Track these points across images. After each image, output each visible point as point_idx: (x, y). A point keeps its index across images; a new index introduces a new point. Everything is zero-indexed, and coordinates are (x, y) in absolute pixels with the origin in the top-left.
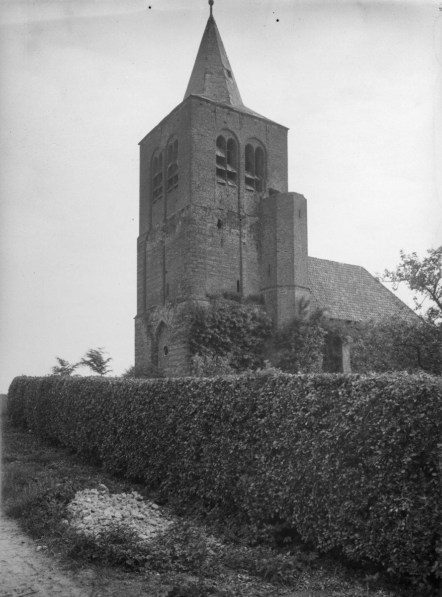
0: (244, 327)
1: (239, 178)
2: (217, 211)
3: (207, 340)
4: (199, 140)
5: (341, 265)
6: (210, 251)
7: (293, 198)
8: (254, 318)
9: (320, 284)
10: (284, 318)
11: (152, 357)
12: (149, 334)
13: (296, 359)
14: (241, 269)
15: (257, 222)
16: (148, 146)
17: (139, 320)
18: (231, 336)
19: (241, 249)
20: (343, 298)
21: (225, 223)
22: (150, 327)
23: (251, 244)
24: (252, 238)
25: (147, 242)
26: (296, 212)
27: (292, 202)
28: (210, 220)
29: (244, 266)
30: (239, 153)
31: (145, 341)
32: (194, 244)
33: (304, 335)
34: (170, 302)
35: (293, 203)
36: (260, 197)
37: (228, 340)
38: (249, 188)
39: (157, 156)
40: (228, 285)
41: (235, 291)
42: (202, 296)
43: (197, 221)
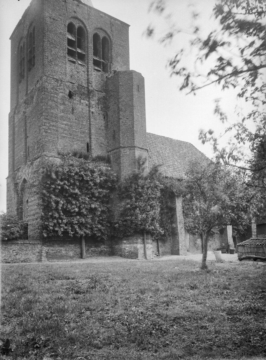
0: (91, 180)
1: (88, 59)
2: (68, 84)
3: (57, 191)
4: (51, 22)
5: (174, 140)
6: (62, 117)
7: (132, 75)
8: (101, 174)
9: (158, 152)
10: (126, 172)
11: (18, 209)
12: (16, 191)
13: (136, 207)
14: (90, 134)
15: (104, 97)
16: (16, 38)
17: (10, 180)
18: (80, 188)
19: (90, 117)
20: (176, 163)
21: (75, 94)
22: (16, 184)
23: (99, 114)
24: (100, 109)
25: (15, 115)
26: (135, 87)
27: (132, 78)
28: (62, 91)
29: (93, 131)
30: (88, 38)
31: (13, 196)
32: (46, 109)
33: (143, 188)
34: (30, 161)
35: (132, 79)
36: (107, 77)
37: (77, 191)
38: (96, 68)
39: (22, 44)
40: (79, 146)
41: (84, 151)
42: (54, 154)
43: (49, 90)
